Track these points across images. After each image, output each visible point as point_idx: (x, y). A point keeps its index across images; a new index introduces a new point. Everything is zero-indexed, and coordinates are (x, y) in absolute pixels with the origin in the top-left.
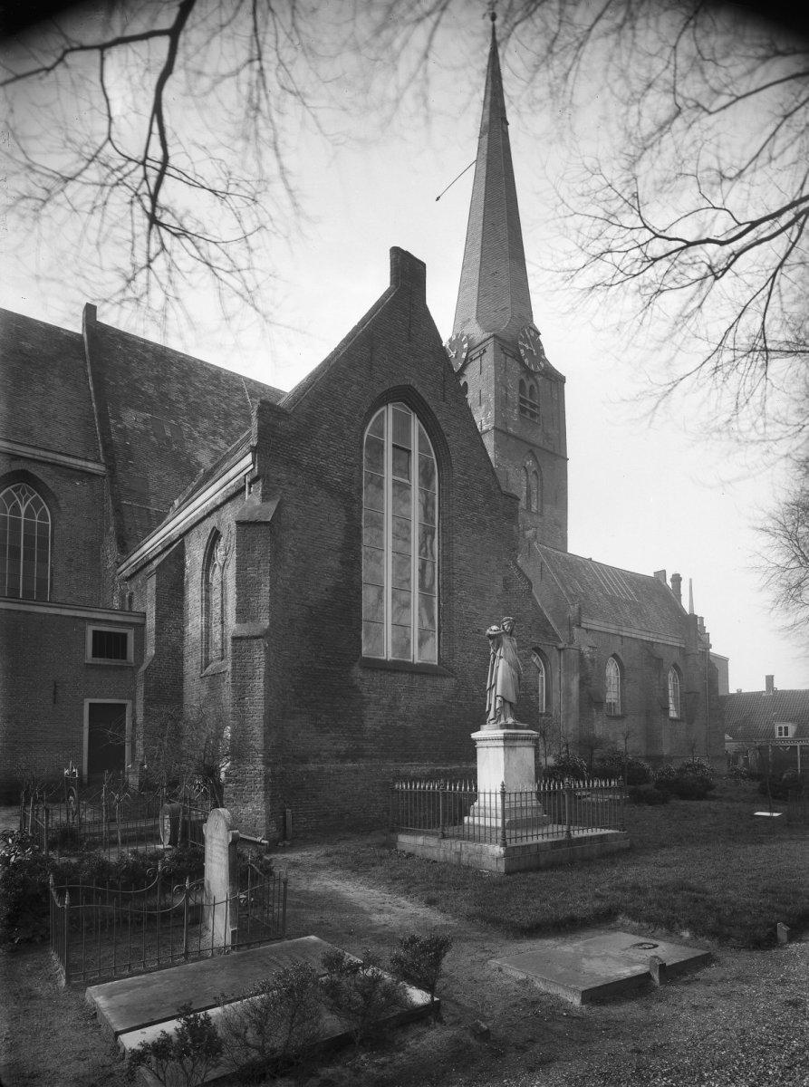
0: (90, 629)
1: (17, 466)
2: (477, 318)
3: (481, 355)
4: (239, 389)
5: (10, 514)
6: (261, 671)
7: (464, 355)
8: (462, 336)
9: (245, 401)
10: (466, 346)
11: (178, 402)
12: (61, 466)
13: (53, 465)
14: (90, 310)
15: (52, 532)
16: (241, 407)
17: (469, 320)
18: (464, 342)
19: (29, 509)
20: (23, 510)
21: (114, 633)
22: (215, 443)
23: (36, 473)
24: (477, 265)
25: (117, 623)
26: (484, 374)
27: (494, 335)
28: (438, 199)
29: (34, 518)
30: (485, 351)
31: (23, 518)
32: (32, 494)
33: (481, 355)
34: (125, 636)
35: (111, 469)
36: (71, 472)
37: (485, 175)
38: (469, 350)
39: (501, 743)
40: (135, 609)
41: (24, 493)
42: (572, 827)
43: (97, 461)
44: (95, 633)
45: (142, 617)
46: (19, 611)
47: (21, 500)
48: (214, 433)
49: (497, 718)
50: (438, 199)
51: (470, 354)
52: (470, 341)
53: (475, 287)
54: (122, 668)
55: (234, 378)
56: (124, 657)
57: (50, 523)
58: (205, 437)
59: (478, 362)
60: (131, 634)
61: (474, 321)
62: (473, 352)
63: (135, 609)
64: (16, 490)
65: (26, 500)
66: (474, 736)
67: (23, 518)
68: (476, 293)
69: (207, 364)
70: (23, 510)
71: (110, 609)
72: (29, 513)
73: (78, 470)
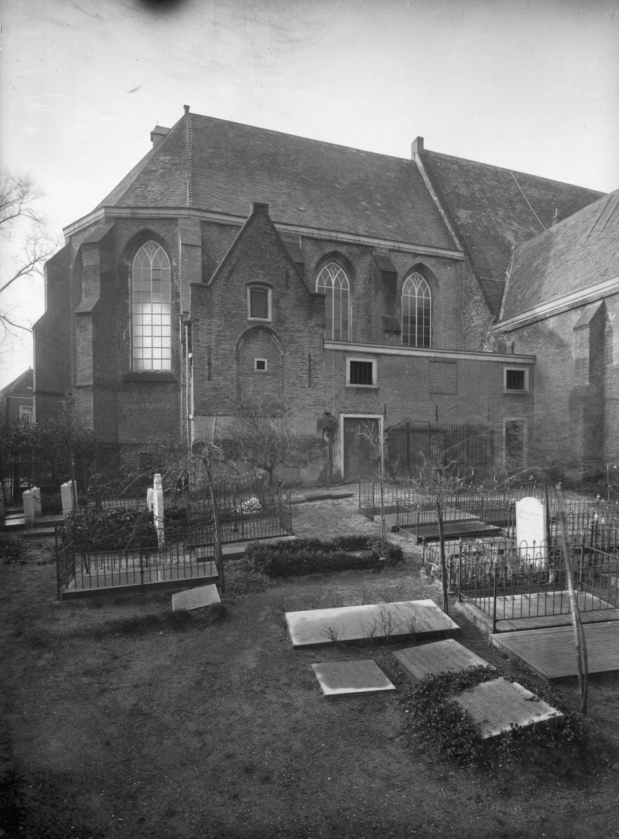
0: (349, 360)
1: (418, 260)
4: (512, 180)
9: (518, 188)
11: (483, 198)
15: (432, 304)
16: (517, 194)
19: (337, 281)
20: (417, 291)
22: (512, 225)
23: (426, 264)
25: (520, 364)
29: (340, 287)
31: (416, 296)
32: (421, 279)
34: (522, 373)
35: (467, 253)
36: (445, 260)
40: (515, 353)
42: (381, 506)
43: (456, 250)
45: (532, 359)
47: (332, 273)
48: (509, 218)
54: (522, 395)
55: (506, 173)
56: (370, 383)
60: (527, 371)
63: (515, 353)
69: (459, 159)
70: (417, 291)
71: (473, 351)
72: (420, 294)
73: (448, 259)
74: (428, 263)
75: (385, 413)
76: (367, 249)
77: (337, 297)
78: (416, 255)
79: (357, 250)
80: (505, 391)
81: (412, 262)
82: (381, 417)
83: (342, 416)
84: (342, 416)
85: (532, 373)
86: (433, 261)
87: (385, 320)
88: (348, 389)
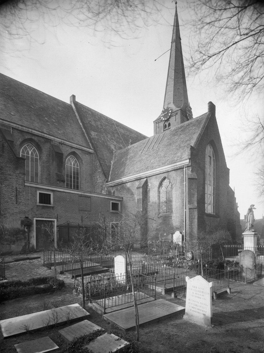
0: (38, 192)
1: (73, 150)
2: (173, 103)
3: (176, 115)
4: (113, 124)
5: (31, 155)
6: (196, 217)
7: (170, 114)
8: (169, 108)
10: (170, 111)
12: (84, 151)
13: (81, 150)
14: (74, 97)
16: (115, 130)
17: (170, 103)
18: (170, 110)
20: (30, 153)
21: (46, 194)
24: (173, 85)
26: (177, 121)
27: (181, 109)
28: (155, 60)
30: (177, 114)
33: (176, 115)
34: (50, 195)
35: (95, 151)
37: (174, 56)
38: (171, 113)
39: (253, 236)
41: (30, 147)
44: (40, 193)
46: (97, 197)
47: (29, 149)
49: (250, 229)
50: (155, 60)
51: (172, 114)
52: (172, 110)
53: (172, 92)
56: (50, 204)
57: (79, 168)
58: (111, 140)
59: (174, 117)
60: (119, 203)
61: (172, 103)
62: (173, 114)
64: (28, 146)
65: (73, 160)
66: (243, 234)
67: (30, 155)
68: (172, 94)
70: (30, 153)
74: (78, 152)
75: (57, 218)
76: (48, 140)
77: (32, 160)
78: (72, 147)
79: (43, 140)
80: (111, 211)
81: (70, 150)
82: (55, 220)
83: (35, 219)
84: (35, 219)
85: (121, 204)
86: (80, 151)
87: (57, 175)
88: (38, 206)
